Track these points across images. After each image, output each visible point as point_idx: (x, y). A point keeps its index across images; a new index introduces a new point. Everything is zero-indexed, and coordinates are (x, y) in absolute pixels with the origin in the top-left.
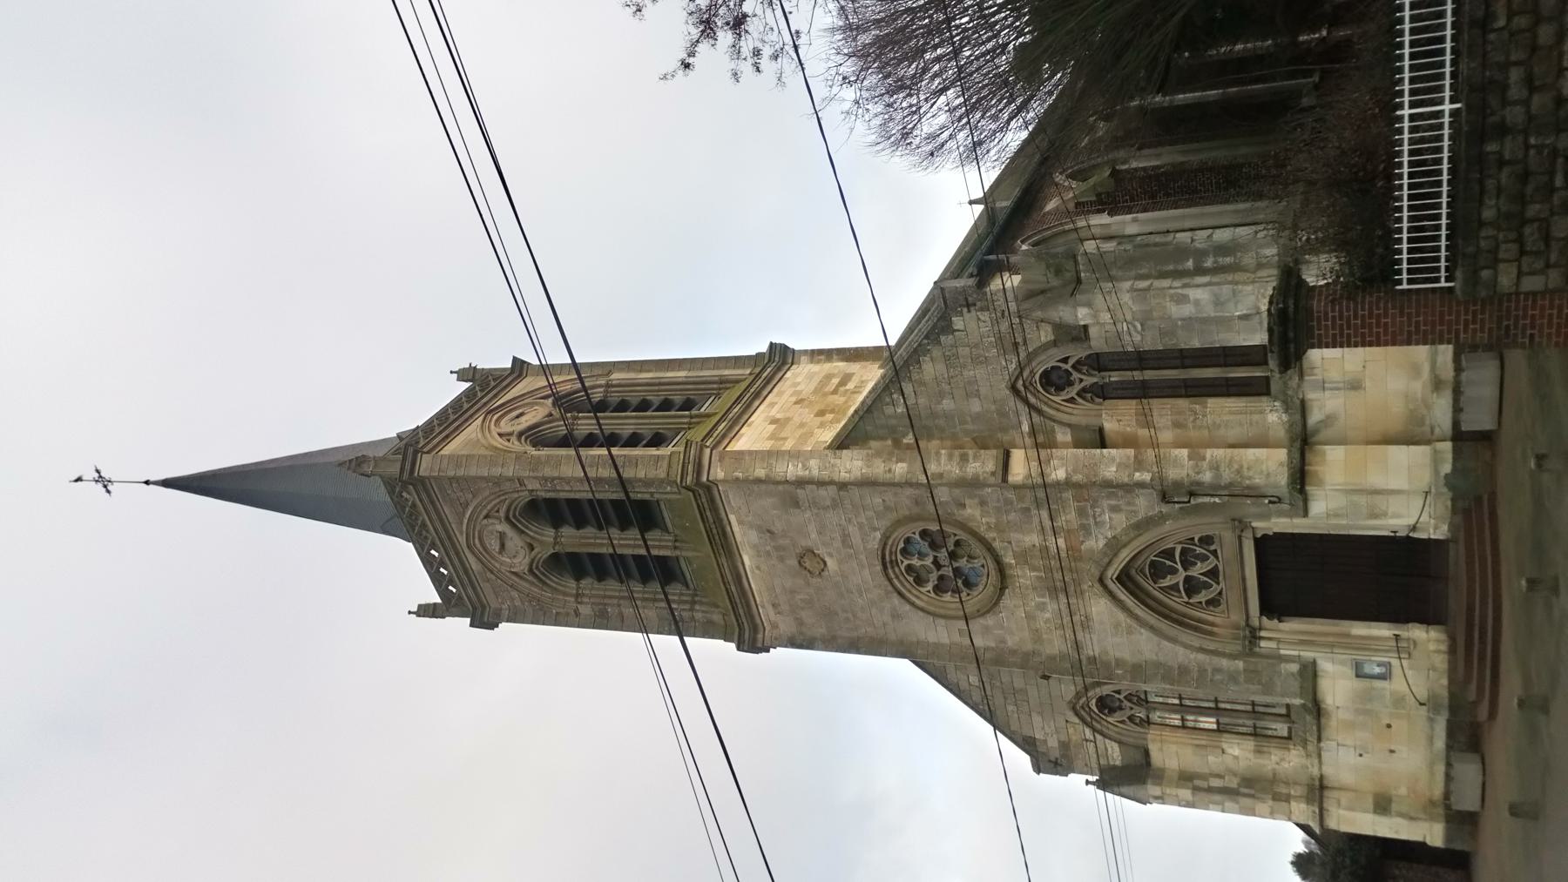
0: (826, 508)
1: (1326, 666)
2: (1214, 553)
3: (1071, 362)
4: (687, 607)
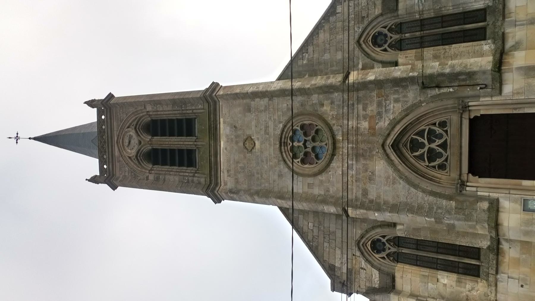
0: (261, 111)
1: (505, 204)
2: (446, 132)
3: (386, 238)
4: (191, 175)
